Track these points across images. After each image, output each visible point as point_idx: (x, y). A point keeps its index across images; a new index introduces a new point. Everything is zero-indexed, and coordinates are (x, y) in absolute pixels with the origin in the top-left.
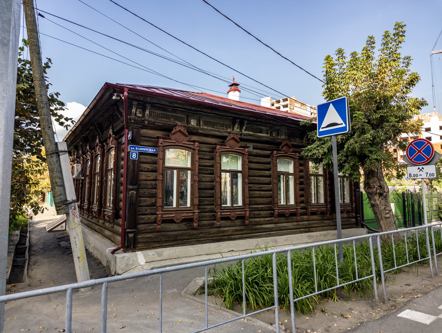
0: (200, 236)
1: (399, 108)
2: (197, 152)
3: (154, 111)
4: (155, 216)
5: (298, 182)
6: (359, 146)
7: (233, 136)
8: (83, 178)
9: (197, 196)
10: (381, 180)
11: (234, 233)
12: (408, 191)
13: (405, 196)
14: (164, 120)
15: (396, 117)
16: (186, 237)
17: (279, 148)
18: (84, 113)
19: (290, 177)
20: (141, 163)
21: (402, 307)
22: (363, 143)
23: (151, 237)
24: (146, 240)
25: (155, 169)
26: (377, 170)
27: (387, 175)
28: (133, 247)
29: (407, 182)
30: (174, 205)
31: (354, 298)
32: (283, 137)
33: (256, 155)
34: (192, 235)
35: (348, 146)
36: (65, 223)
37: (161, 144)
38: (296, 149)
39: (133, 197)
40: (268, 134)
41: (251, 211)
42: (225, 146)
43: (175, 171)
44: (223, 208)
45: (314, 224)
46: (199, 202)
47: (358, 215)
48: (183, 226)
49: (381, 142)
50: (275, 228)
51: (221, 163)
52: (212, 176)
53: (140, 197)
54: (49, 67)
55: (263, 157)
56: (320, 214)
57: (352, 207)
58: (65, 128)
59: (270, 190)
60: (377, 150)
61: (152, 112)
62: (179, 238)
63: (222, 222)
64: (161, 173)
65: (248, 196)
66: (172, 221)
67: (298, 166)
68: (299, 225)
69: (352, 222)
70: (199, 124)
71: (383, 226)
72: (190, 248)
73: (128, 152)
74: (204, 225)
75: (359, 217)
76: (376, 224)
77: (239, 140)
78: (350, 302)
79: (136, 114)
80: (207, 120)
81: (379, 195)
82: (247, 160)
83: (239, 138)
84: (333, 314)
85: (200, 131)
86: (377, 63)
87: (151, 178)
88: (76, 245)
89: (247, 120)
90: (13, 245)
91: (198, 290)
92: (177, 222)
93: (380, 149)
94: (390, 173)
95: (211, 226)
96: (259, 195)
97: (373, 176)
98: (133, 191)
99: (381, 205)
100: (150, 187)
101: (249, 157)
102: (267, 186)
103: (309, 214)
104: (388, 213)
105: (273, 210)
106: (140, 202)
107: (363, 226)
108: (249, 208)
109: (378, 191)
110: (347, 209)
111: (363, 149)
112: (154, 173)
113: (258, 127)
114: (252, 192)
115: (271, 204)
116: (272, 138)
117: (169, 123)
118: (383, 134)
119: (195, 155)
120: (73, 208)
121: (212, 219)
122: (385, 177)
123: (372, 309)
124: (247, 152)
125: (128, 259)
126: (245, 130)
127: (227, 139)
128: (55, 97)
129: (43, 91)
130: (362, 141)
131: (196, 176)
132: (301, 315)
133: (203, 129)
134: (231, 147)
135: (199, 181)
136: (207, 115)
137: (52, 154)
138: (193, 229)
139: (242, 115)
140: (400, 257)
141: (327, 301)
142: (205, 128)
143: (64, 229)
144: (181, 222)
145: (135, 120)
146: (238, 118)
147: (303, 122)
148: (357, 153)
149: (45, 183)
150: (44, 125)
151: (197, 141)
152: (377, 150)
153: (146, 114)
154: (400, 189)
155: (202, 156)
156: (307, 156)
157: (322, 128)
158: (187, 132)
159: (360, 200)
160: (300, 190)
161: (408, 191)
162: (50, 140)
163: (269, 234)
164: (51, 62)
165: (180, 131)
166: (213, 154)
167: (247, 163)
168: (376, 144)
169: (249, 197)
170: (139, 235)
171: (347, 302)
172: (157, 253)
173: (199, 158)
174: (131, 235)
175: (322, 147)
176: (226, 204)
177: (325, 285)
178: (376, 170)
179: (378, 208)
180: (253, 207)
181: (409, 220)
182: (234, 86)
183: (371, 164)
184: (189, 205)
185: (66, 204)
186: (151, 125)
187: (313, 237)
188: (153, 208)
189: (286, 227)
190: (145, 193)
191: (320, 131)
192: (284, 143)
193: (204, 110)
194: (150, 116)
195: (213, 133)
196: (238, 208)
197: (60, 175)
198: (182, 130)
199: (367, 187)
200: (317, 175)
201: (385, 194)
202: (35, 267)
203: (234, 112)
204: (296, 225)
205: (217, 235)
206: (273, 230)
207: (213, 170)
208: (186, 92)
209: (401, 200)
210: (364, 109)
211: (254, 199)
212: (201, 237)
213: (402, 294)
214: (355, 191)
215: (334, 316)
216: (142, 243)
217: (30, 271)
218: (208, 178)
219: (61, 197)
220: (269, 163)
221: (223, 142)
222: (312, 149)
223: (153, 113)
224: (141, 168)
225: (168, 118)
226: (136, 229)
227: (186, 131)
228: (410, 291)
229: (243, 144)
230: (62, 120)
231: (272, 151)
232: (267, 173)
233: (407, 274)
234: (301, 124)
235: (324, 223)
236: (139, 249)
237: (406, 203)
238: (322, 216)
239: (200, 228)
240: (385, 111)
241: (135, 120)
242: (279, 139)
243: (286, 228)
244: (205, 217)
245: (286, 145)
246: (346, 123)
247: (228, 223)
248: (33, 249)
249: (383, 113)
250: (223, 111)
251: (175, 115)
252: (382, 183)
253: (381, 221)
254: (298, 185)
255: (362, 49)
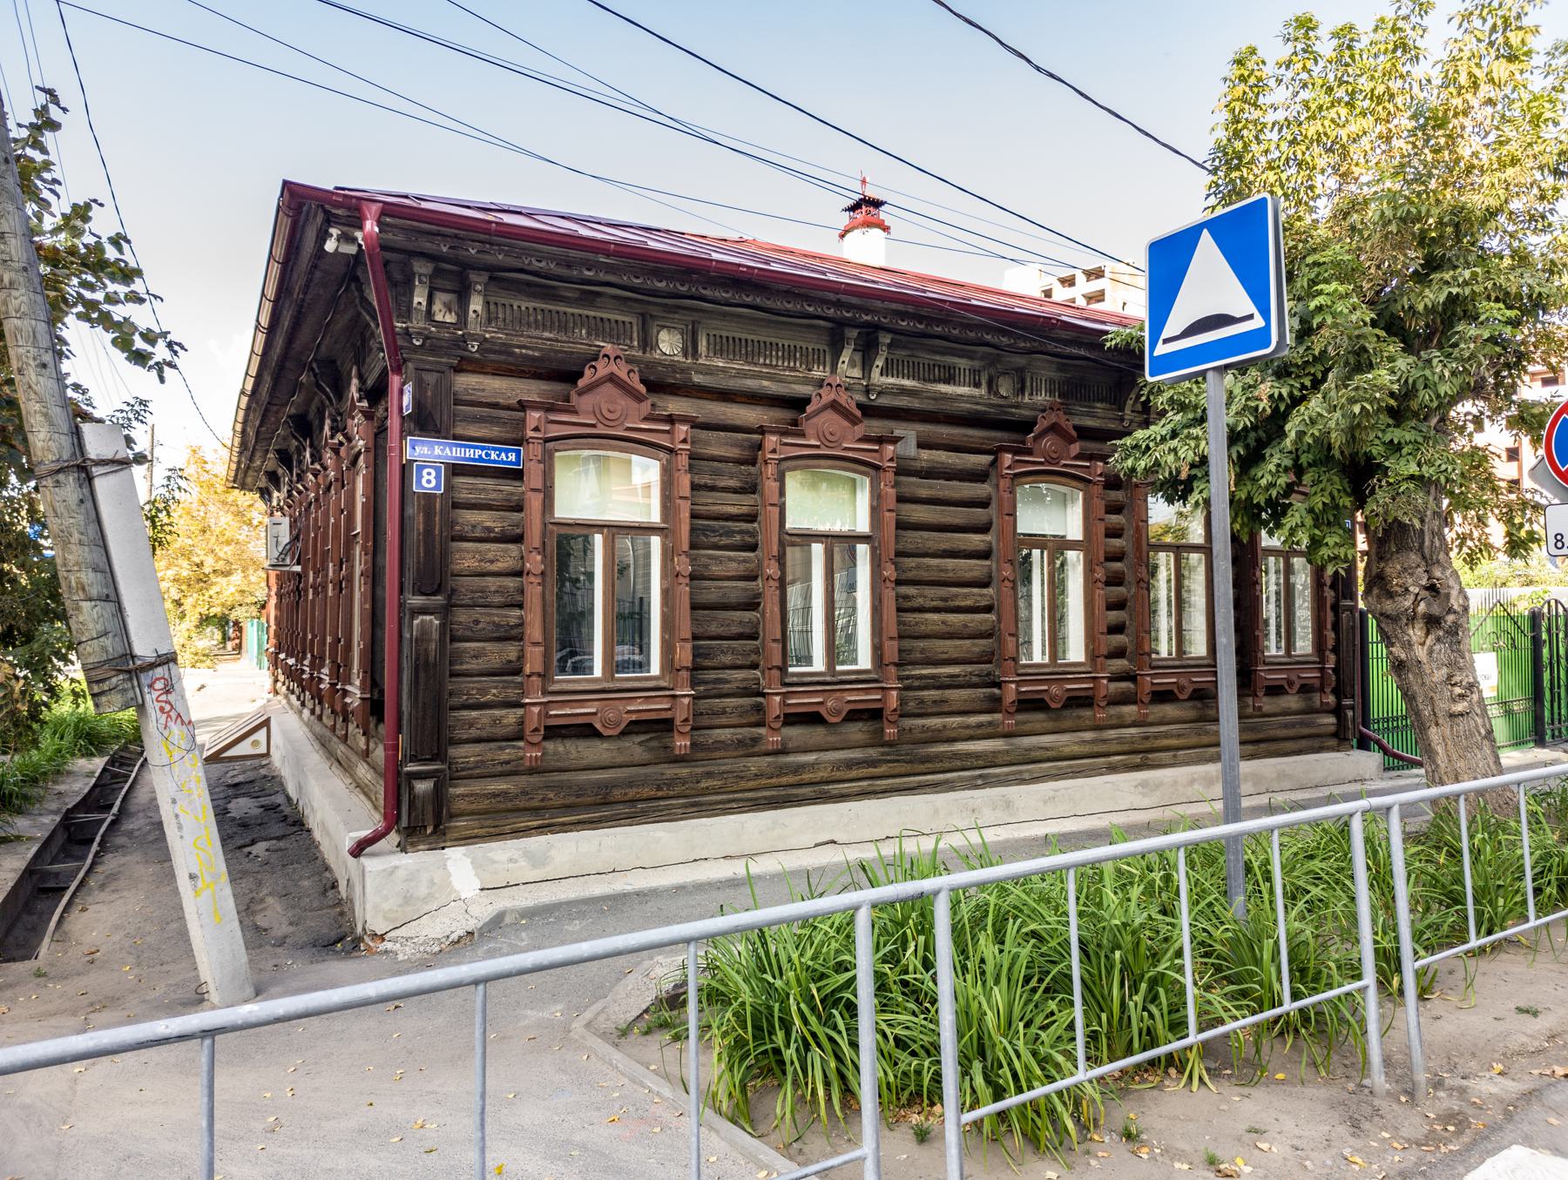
0: (703, 785)
1: (1522, 259)
2: (683, 460)
3: (506, 302)
4: (520, 712)
5: (1100, 574)
6: (1344, 423)
7: (832, 396)
8: (298, 569)
9: (689, 636)
10: (1438, 562)
11: (838, 775)
12: (1553, 603)
13: (1540, 625)
14: (546, 334)
15: (1505, 298)
16: (647, 792)
17: (1023, 442)
18: (258, 320)
19: (1073, 556)
20: (456, 506)
21: (1495, 1128)
22: (1357, 409)
23: (505, 793)
24: (484, 804)
25: (518, 531)
26: (1422, 521)
27: (1463, 539)
28: (434, 832)
29: (1553, 569)
30: (598, 672)
31: (1283, 1068)
32: (1042, 398)
33: (930, 473)
34: (672, 782)
35: (1302, 428)
36: (265, 729)
37: (536, 429)
38: (1093, 447)
39: (430, 640)
40: (977, 385)
41: (906, 688)
42: (802, 435)
43: (598, 539)
44: (795, 679)
45: (1166, 735)
46: (694, 656)
47: (1347, 702)
48: (634, 748)
49: (1438, 407)
50: (1007, 752)
51: (784, 504)
52: (751, 554)
53: (454, 639)
54: (54, 126)
55: (960, 480)
56: (1190, 699)
57: (1322, 670)
58: (154, 373)
59: (988, 609)
60: (1420, 440)
61: (496, 304)
62: (617, 794)
63: (795, 733)
64: (537, 543)
65: (894, 633)
66: (587, 731)
67: (1101, 512)
68: (1104, 741)
69: (1322, 730)
70: (691, 349)
71: (1440, 749)
72: (660, 834)
73: (403, 467)
74: (720, 745)
75: (1352, 708)
76: (1411, 736)
77: (858, 413)
78: (1258, 1093)
79: (429, 313)
80: (724, 334)
81: (1427, 623)
82: (892, 492)
83: (860, 406)
84: (1171, 1153)
85: (697, 379)
86: (1437, 77)
87: (500, 565)
88: (180, 828)
89: (889, 331)
90: (55, 813)
91: (646, 1011)
92: (606, 733)
93: (1433, 432)
94: (1476, 534)
95: (749, 747)
96: (943, 627)
97: (1403, 547)
98: (428, 618)
99: (1434, 666)
100: (497, 599)
101: (902, 479)
102: (975, 590)
103: (1146, 699)
104: (1459, 695)
105: (999, 685)
106: (455, 658)
107: (1364, 744)
108: (900, 679)
109: (1422, 607)
110: (1299, 677)
111: (1357, 434)
112: (511, 546)
113: (938, 358)
114: (910, 617)
115: (990, 662)
116: (995, 400)
117: (567, 347)
118: (1447, 374)
119: (677, 474)
120: (159, 685)
121: (752, 719)
122: (1456, 550)
123: (1353, 1135)
124: (891, 460)
125: (412, 877)
126: (885, 372)
127: (809, 409)
128: (111, 253)
129: (10, 217)
130: (1352, 401)
131: (683, 557)
132: (1029, 1156)
133: (709, 371)
134: (826, 441)
135: (693, 577)
136: (725, 315)
137: (58, 471)
138: (676, 761)
139: (867, 311)
140: (1499, 886)
141: (1159, 1087)
142: (716, 366)
143: (263, 750)
144: (623, 733)
145: (426, 338)
146: (852, 324)
147: (1118, 334)
148: (1336, 453)
149: (232, 589)
150: (19, 358)
151: (684, 419)
152: (1420, 440)
153: (471, 313)
154: (1523, 600)
155: (706, 479)
156: (1133, 470)
157: (1166, 341)
158: (642, 381)
159: (1358, 642)
160: (1111, 607)
161: (1553, 603)
162: (46, 415)
163: (980, 776)
164: (58, 104)
165: (612, 379)
166: (752, 469)
167: (892, 503)
168: (1416, 415)
169: (901, 637)
170: (455, 786)
171: (1246, 1090)
172: (527, 854)
173: (695, 487)
174: (423, 787)
175: (1188, 436)
176: (808, 660)
177: (1151, 1016)
178: (1417, 525)
179: (1421, 674)
180: (918, 672)
181: (1552, 719)
182: (866, 208)
183: (1394, 500)
184: (655, 669)
185: (129, 672)
186: (492, 356)
187: (1159, 785)
188: (513, 682)
189: (1052, 749)
190: (477, 622)
191: (1155, 354)
192: (1046, 423)
193: (707, 293)
194: (489, 321)
195: (751, 384)
196: (853, 677)
197: (96, 556)
198: (623, 374)
199: (1376, 591)
200: (1178, 547)
201: (1451, 618)
202: (103, 896)
203: (832, 296)
204: (1093, 742)
205: (774, 781)
206: (999, 760)
207: (753, 534)
208: (667, 231)
209: (1525, 643)
210: (1372, 271)
211: (921, 644)
212: (706, 792)
213: (1496, 1056)
214: (1335, 608)
215: (1177, 1165)
216: (468, 815)
217: (75, 912)
218: (734, 565)
219: (107, 642)
220: (984, 504)
221: (795, 423)
222: (1151, 444)
223: (500, 309)
224: (457, 528)
225: (563, 328)
226: (443, 762)
227: (636, 378)
228: (1536, 1044)
229: (877, 427)
230: (139, 344)
231: (996, 452)
232: (976, 540)
233: (1530, 958)
234: (1108, 344)
235: (1207, 733)
236: (456, 840)
237: (1545, 651)
238: (1199, 705)
239: (701, 755)
240: (1467, 274)
241: (426, 338)
242: (1026, 406)
243: (1049, 754)
244: (724, 713)
245: (1054, 428)
246: (1265, 313)
247: (817, 734)
248: (128, 825)
249: (1459, 285)
250: (787, 292)
251: (592, 313)
252: (1438, 574)
253: (1433, 730)
254: (1100, 585)
255: (1373, 27)
